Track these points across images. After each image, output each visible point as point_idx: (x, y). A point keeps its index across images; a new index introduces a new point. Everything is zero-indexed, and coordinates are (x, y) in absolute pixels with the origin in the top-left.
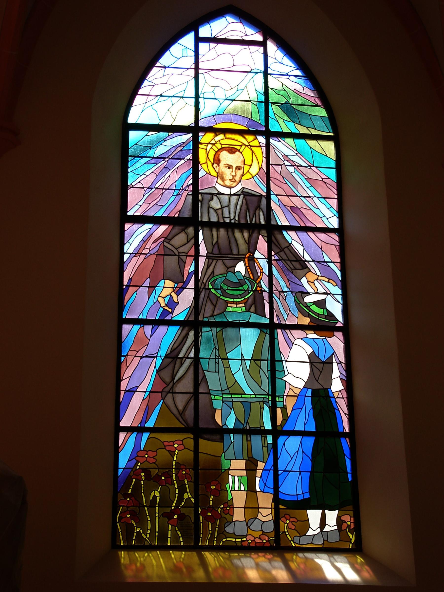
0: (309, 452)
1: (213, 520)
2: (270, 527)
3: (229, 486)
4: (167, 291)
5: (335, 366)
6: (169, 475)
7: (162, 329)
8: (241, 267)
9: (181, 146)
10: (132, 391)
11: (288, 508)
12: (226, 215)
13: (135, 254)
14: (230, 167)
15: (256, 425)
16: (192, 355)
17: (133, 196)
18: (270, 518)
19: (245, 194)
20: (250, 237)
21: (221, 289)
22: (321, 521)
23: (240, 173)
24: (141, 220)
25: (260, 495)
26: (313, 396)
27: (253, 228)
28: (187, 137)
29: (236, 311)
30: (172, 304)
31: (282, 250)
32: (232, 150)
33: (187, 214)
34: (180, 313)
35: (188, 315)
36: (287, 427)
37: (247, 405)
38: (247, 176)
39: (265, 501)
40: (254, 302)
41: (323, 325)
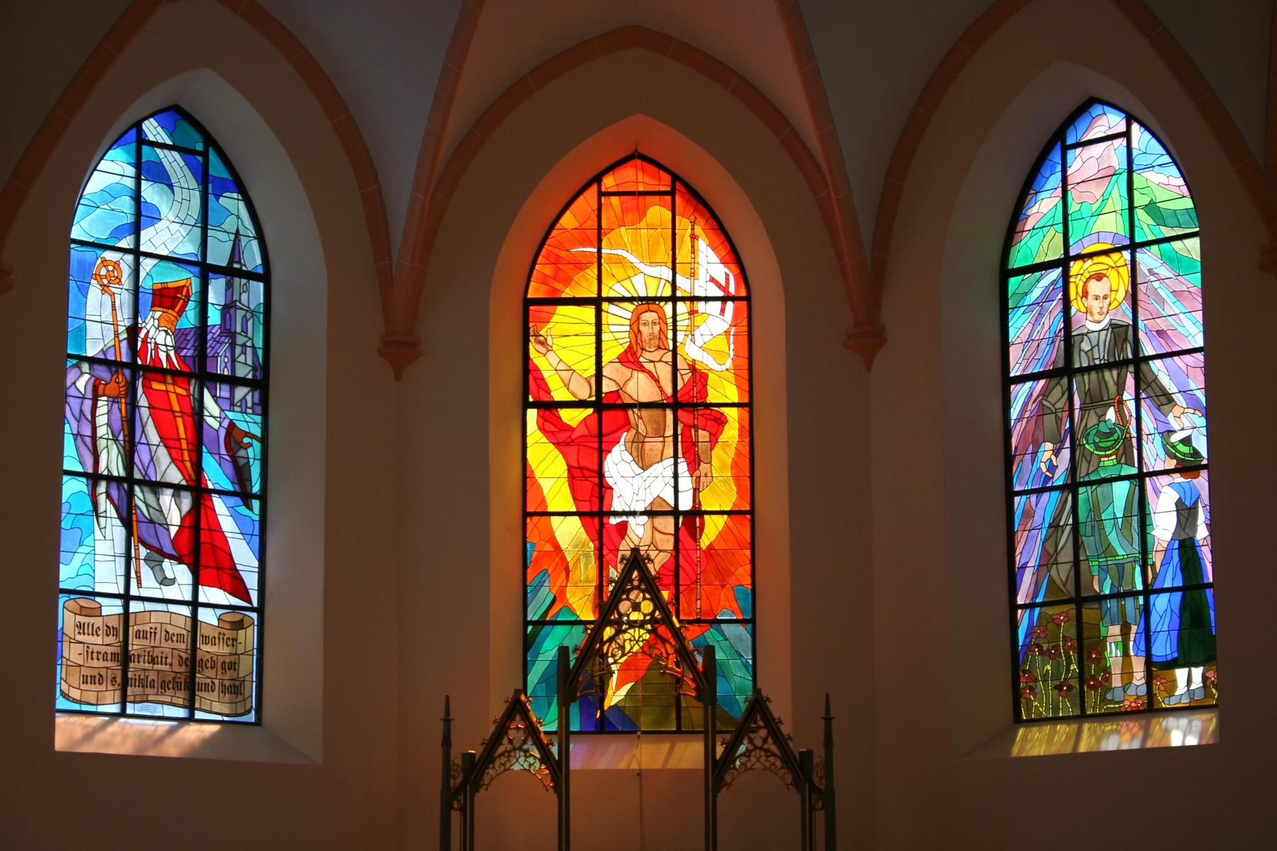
0: (1177, 610)
1: (1094, 688)
2: (1143, 691)
3: (1107, 654)
4: (1048, 455)
5: (1200, 510)
6: (1057, 648)
7: (1046, 496)
8: (1111, 414)
9: (812, 809)
10: (1024, 567)
11: (1157, 669)
12: (1096, 356)
13: (1019, 419)
14: (1097, 298)
15: (1128, 588)
16: (1071, 521)
17: (1014, 353)
18: (1143, 681)
19: (1114, 327)
21: (1094, 442)
22: (1188, 680)
23: (1107, 302)
24: (1022, 379)
26: (1180, 548)
27: (1121, 365)
28: (1056, 273)
29: (1109, 465)
30: (1052, 468)
31: (1149, 385)
32: (1099, 277)
33: (1061, 364)
34: (1059, 479)
35: (1066, 479)
36: (1157, 586)
37: (1120, 567)
39: (1138, 665)
40: (1124, 453)
41: (1187, 467)
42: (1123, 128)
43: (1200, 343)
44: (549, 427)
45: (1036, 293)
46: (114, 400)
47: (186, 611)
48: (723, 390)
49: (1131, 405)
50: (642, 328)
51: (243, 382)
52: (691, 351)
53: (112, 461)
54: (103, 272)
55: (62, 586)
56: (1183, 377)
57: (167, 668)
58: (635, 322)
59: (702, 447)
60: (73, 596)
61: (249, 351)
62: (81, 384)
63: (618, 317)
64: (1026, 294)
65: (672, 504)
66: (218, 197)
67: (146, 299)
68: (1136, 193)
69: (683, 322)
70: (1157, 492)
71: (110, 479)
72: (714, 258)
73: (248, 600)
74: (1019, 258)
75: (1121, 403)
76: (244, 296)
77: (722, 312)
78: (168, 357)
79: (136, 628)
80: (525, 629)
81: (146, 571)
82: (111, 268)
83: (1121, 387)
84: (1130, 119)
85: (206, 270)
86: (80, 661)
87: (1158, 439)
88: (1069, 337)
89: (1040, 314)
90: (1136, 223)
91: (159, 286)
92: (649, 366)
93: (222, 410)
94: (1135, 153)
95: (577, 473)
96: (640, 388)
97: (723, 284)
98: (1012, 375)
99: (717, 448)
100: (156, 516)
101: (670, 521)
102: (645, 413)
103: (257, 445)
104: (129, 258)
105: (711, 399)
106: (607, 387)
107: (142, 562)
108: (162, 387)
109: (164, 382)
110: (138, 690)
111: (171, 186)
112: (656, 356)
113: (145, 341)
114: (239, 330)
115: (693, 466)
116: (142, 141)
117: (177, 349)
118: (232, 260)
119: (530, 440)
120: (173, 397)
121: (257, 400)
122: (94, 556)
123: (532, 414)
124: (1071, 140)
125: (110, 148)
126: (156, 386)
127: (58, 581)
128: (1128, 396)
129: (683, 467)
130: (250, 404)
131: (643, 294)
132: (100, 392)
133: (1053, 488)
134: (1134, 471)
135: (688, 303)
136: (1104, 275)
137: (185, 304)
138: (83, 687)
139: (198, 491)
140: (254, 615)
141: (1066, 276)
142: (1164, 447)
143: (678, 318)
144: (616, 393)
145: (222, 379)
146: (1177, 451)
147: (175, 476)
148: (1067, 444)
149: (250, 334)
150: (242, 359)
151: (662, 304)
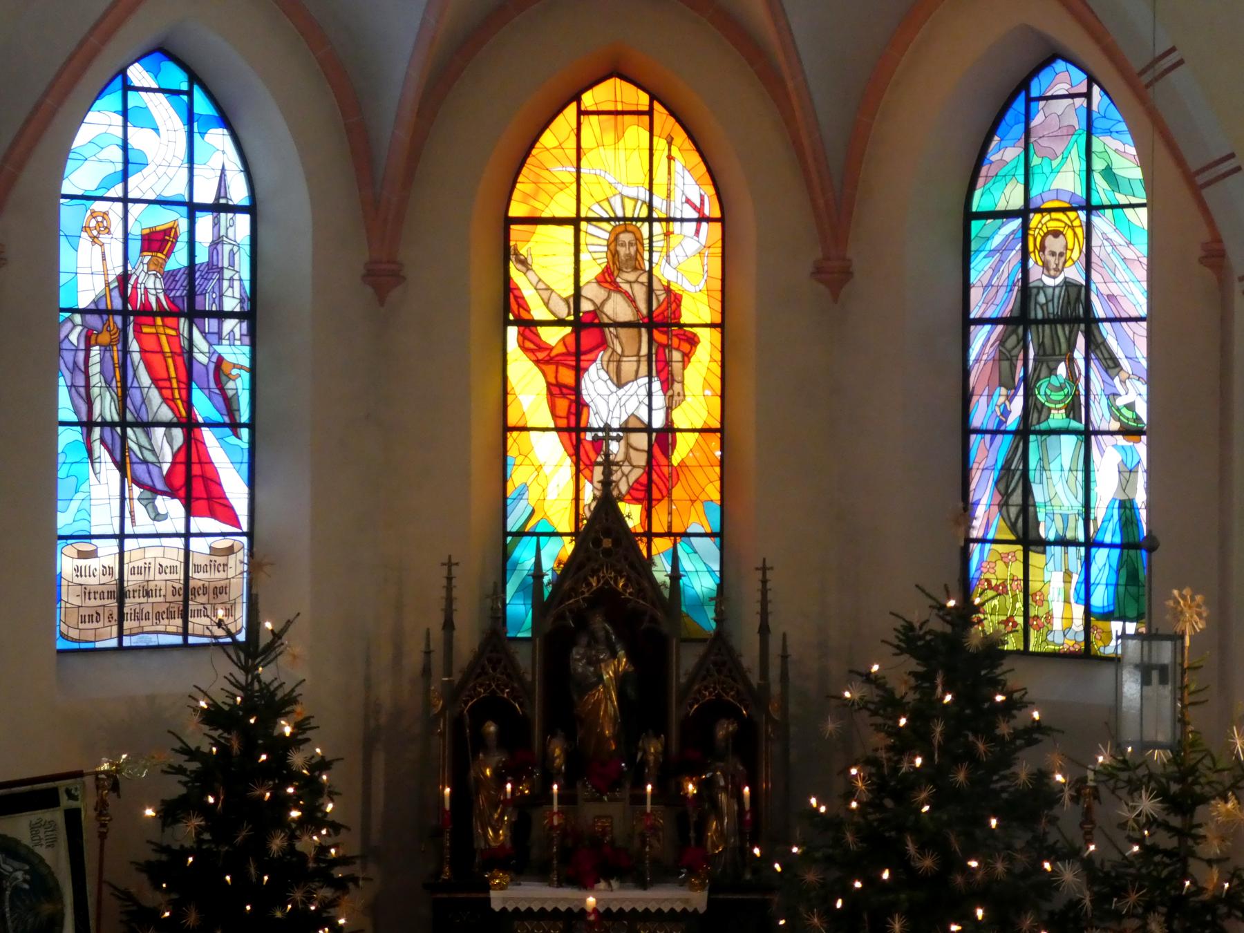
0: (1115, 565)
2: (1081, 638)
6: (1005, 587)
7: (999, 437)
8: (1062, 369)
10: (977, 503)
12: (1051, 310)
13: (977, 360)
14: (1053, 254)
17: (976, 295)
20: (1071, 332)
21: (1046, 394)
23: (1062, 259)
24: (982, 321)
25: (1074, 605)
28: (1016, 223)
30: (1006, 413)
32: (1056, 234)
35: (1018, 426)
37: (1065, 518)
38: (1070, 262)
42: (1084, 89)
43: (1143, 312)
44: (529, 345)
45: (997, 241)
46: (106, 348)
47: (180, 542)
48: (698, 309)
49: (1081, 363)
50: (619, 248)
51: (231, 315)
52: (664, 273)
53: (106, 407)
54: (93, 223)
55: (61, 532)
56: (1131, 345)
57: (162, 599)
58: (613, 242)
59: (677, 367)
60: (70, 541)
61: (236, 284)
62: (73, 338)
63: (596, 238)
64: (988, 239)
65: (646, 420)
66: (202, 134)
67: (135, 246)
68: (1094, 156)
69: (659, 243)
70: (1102, 452)
71: (104, 424)
72: (689, 179)
73: (238, 525)
74: (980, 202)
75: (1071, 362)
76: (231, 231)
77: (697, 232)
78: (158, 300)
79: (131, 565)
80: (505, 540)
81: (139, 509)
82: (100, 219)
83: (1072, 346)
84: (1091, 80)
85: (193, 209)
86: (77, 602)
87: (1104, 401)
88: (1026, 291)
89: (1001, 261)
90: (1093, 186)
91: (147, 231)
92: (626, 287)
93: (210, 345)
94: (1095, 115)
95: (556, 390)
96: (617, 309)
97: (698, 205)
98: (972, 316)
99: (690, 367)
100: (149, 457)
101: (644, 436)
102: (623, 332)
103: (246, 376)
104: (120, 205)
105: (683, 320)
106: (586, 306)
107: (136, 502)
108: (153, 330)
109: (154, 325)
110: (135, 624)
111: (156, 130)
112: (631, 276)
113: (135, 287)
114: (226, 264)
115: (667, 385)
116: (127, 87)
117: (166, 291)
118: (218, 197)
119: (510, 357)
120: (163, 339)
121: (245, 331)
122: (91, 494)
123: (512, 332)
124: (1034, 93)
125: (97, 98)
126: (146, 330)
127: (56, 529)
128: (1079, 355)
129: (656, 385)
130: (238, 336)
131: (620, 214)
132: (93, 342)
133: (1005, 432)
134: (1081, 426)
135: (664, 224)
136: (1061, 233)
137: (174, 245)
138: (81, 626)
139: (189, 425)
140: (244, 540)
141: (1025, 227)
142: (1109, 408)
143: (655, 239)
144: (594, 313)
145: (211, 314)
146: (1121, 414)
147: (166, 414)
148: (1021, 392)
149: (237, 268)
150: (229, 293)
151: (639, 224)
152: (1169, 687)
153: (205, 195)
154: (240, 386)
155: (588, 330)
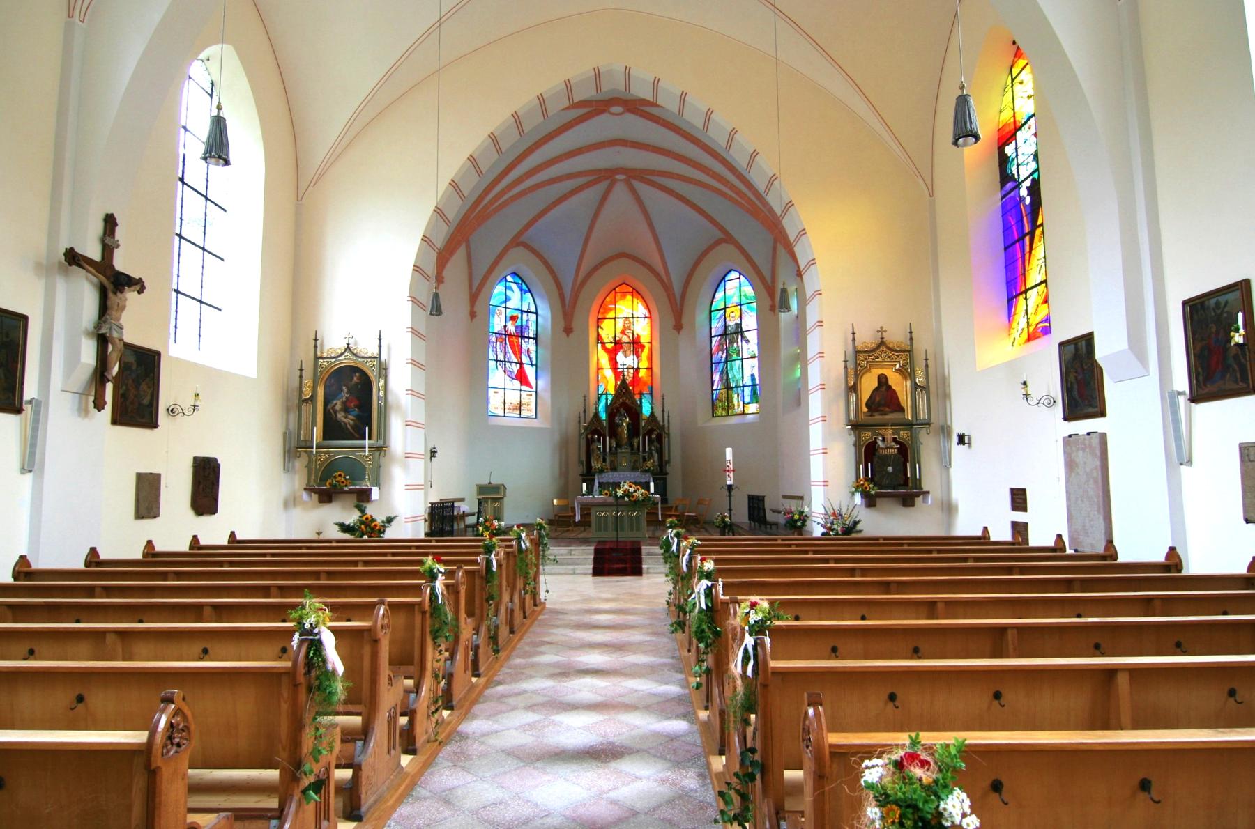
53: (501, 357)
56: (752, 336)
85: (522, 312)
88: (726, 327)
96: (625, 339)
139: (521, 364)
152: (10, 580)
153: (525, 309)
154: (533, 355)
155: (618, 345)
